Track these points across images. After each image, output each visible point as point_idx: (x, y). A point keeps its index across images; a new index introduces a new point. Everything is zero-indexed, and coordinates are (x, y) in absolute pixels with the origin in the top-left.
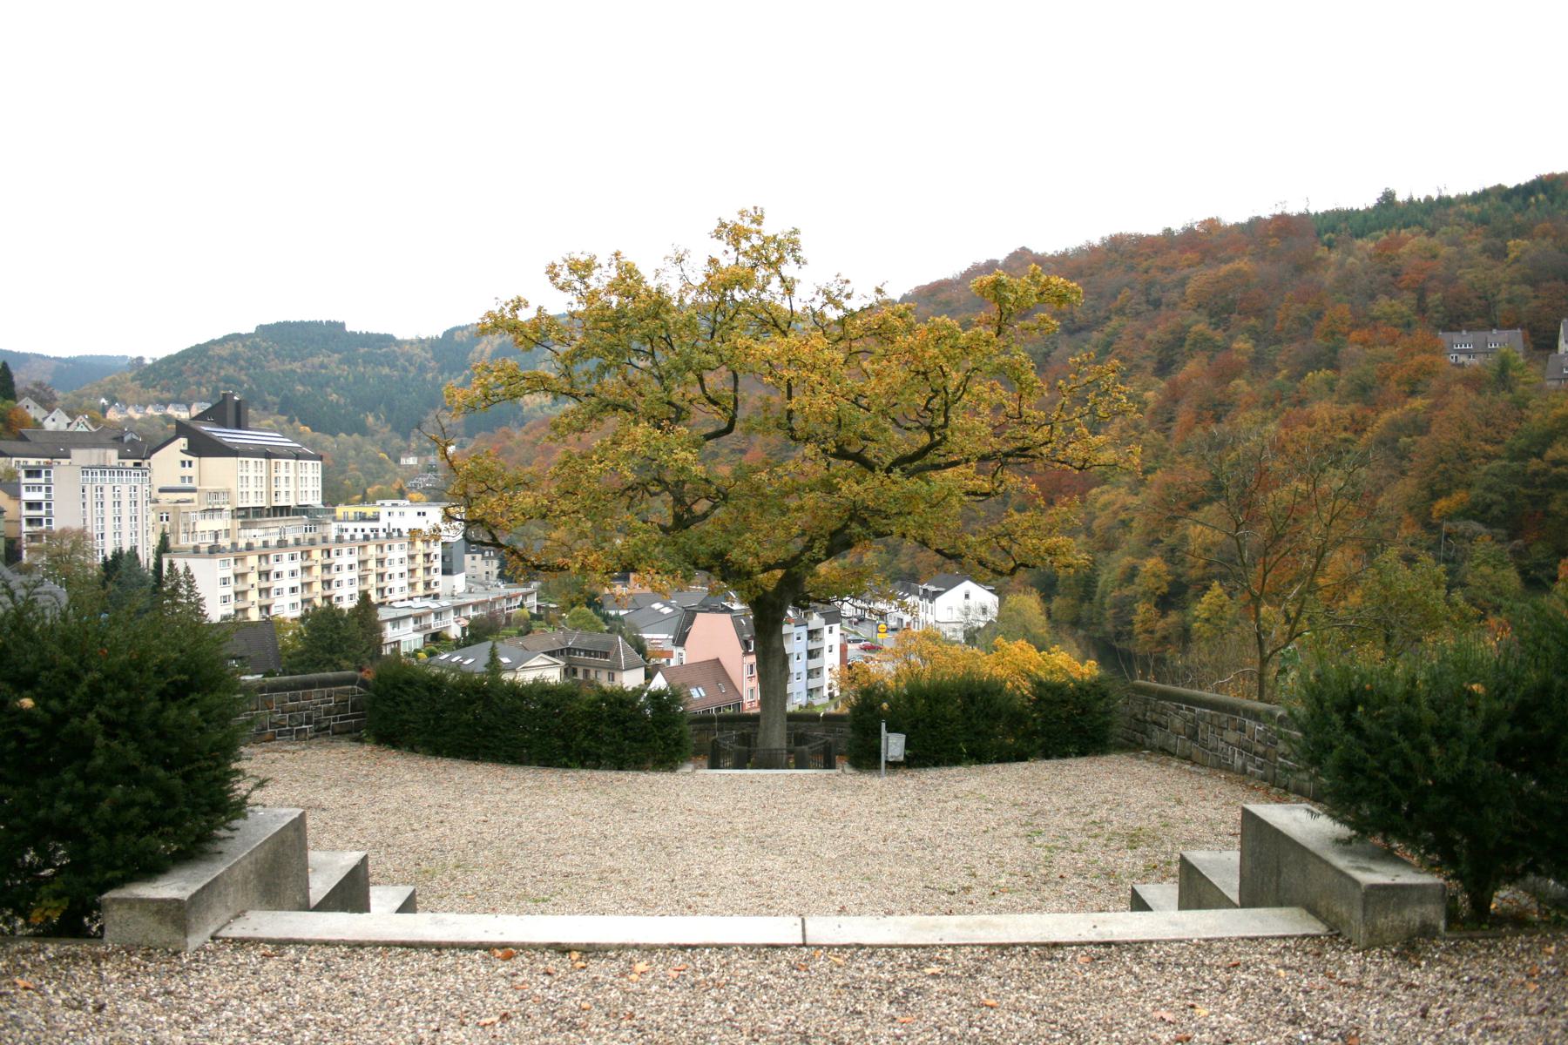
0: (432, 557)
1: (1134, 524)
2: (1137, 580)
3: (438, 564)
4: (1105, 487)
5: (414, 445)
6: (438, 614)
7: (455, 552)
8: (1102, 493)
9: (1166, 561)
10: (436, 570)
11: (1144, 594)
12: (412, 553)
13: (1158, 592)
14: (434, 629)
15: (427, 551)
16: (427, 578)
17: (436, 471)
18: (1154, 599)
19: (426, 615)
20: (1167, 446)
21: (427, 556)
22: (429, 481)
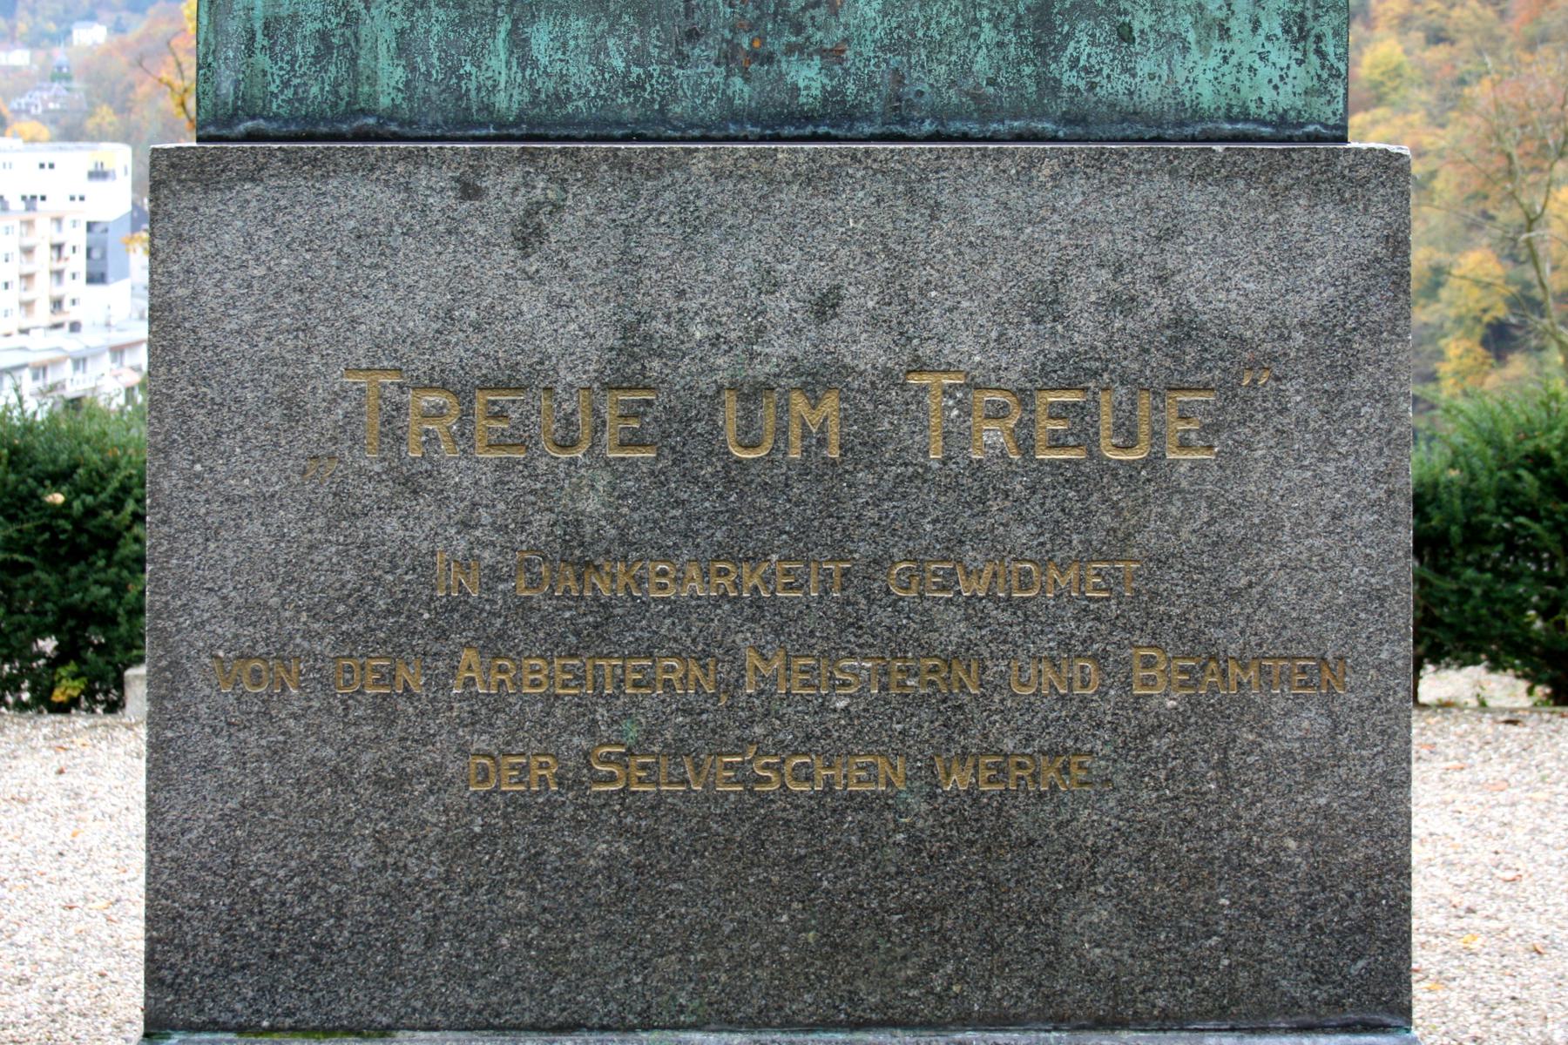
0: (67, 251)
1: (1438, 184)
2: (1444, 293)
3: (77, 263)
4: (1380, 112)
5: (22, 27)
6: (79, 362)
7: (113, 239)
8: (1375, 123)
9: (1500, 258)
10: (74, 276)
11: (1459, 320)
12: (27, 242)
13: (1487, 318)
14: (71, 392)
15: (57, 239)
16: (57, 291)
17: (68, 78)
18: (1479, 331)
19: (56, 363)
20: (1500, 30)
21: (58, 248)
22: (55, 98)
